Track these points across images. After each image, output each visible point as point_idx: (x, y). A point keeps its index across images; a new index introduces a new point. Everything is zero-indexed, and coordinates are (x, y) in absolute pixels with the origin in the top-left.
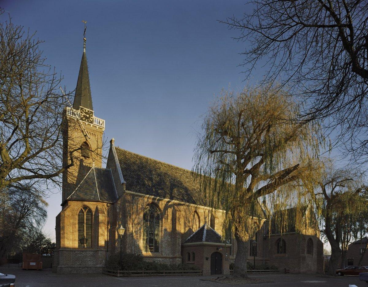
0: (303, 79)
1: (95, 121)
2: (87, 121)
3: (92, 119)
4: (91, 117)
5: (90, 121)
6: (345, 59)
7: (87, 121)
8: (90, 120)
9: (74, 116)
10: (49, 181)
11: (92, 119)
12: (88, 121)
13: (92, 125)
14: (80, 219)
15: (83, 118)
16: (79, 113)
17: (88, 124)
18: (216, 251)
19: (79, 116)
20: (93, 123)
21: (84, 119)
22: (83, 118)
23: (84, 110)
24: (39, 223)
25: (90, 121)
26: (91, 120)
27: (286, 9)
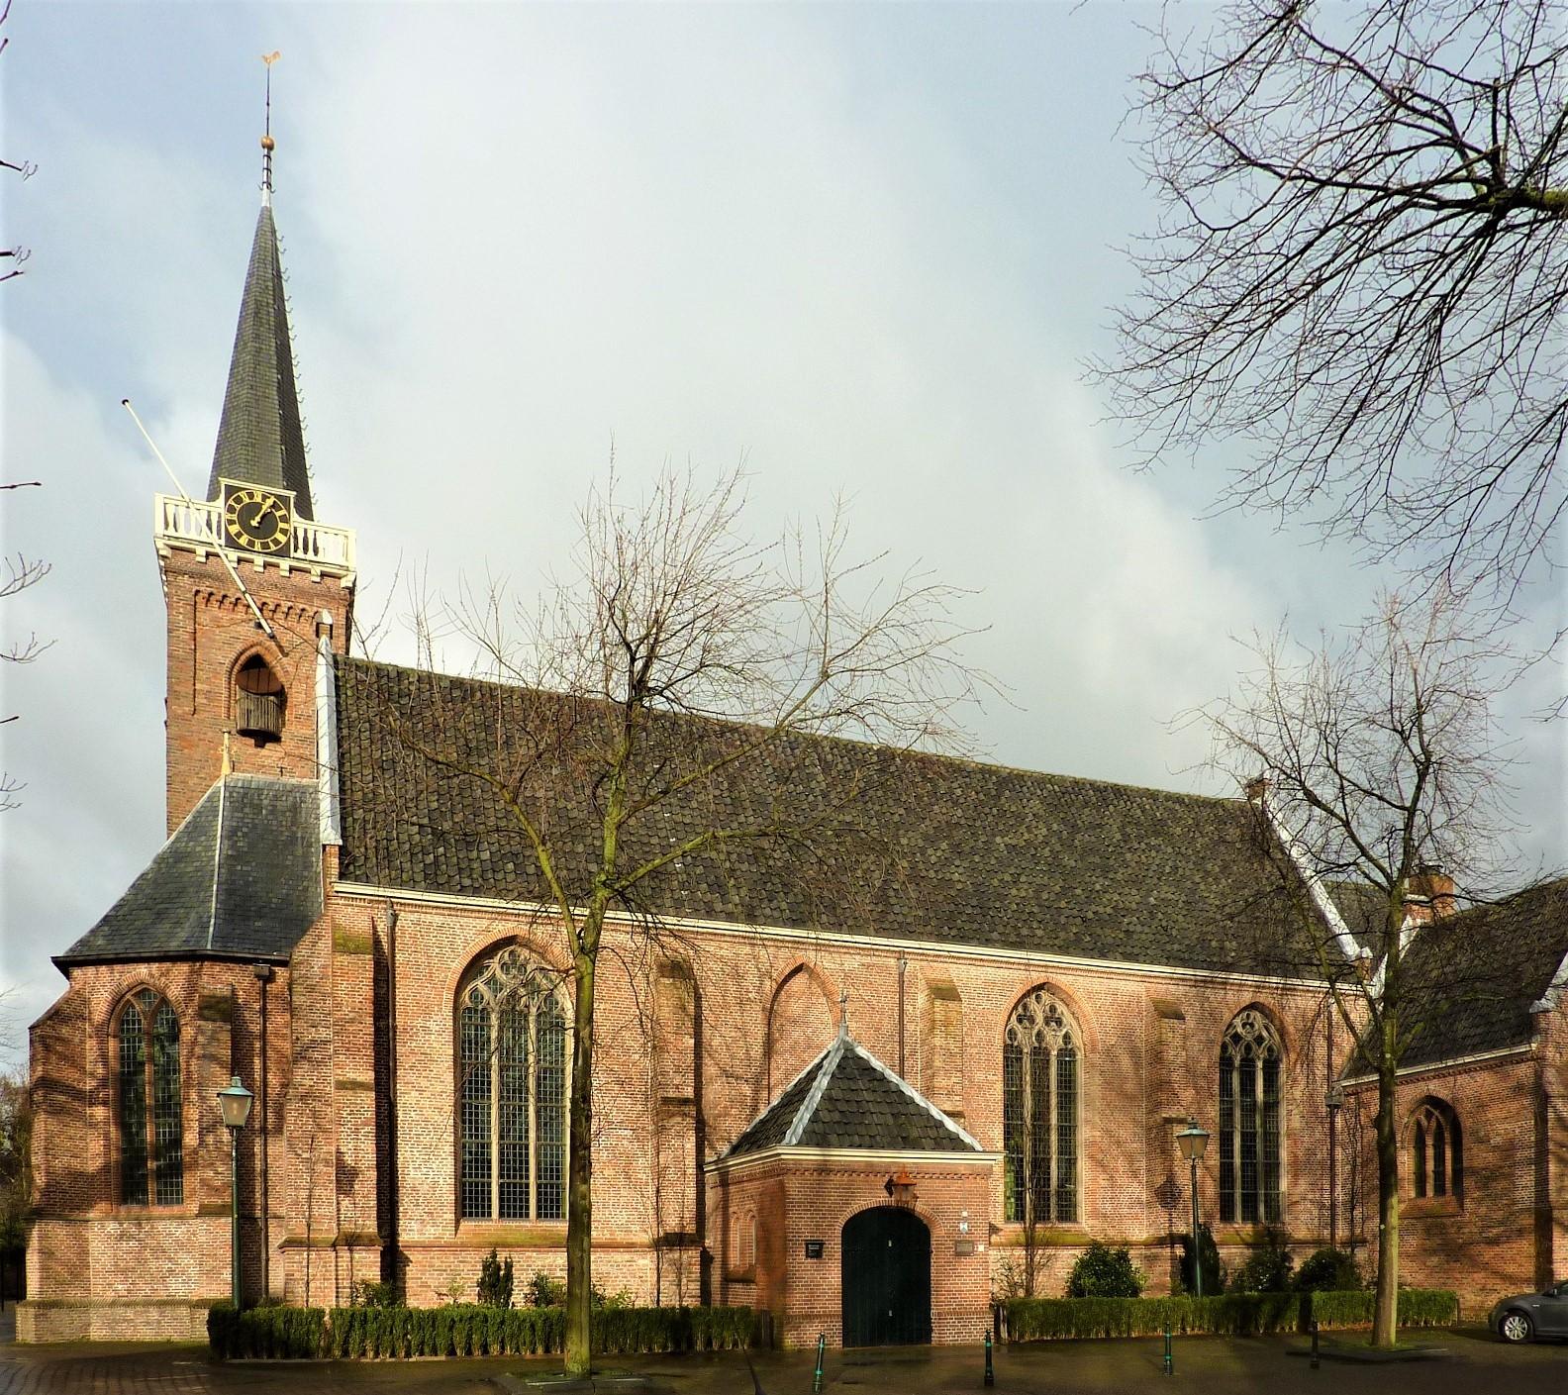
0: (1509, 346)
1: (301, 545)
2: (258, 547)
4: (281, 525)
5: (273, 548)
6: (1183, 163)
7: (258, 547)
8: (276, 542)
9: (310, 555)
10: (778, 1046)
11: (284, 532)
12: (265, 546)
14: (521, 1193)
15: (239, 535)
16: (220, 515)
17: (240, 560)
18: (880, 1198)
19: (219, 533)
20: (292, 554)
21: (243, 541)
22: (239, 535)
23: (242, 494)
24: (472, 1317)
25: (273, 548)
26: (282, 539)
27: (1472, 155)
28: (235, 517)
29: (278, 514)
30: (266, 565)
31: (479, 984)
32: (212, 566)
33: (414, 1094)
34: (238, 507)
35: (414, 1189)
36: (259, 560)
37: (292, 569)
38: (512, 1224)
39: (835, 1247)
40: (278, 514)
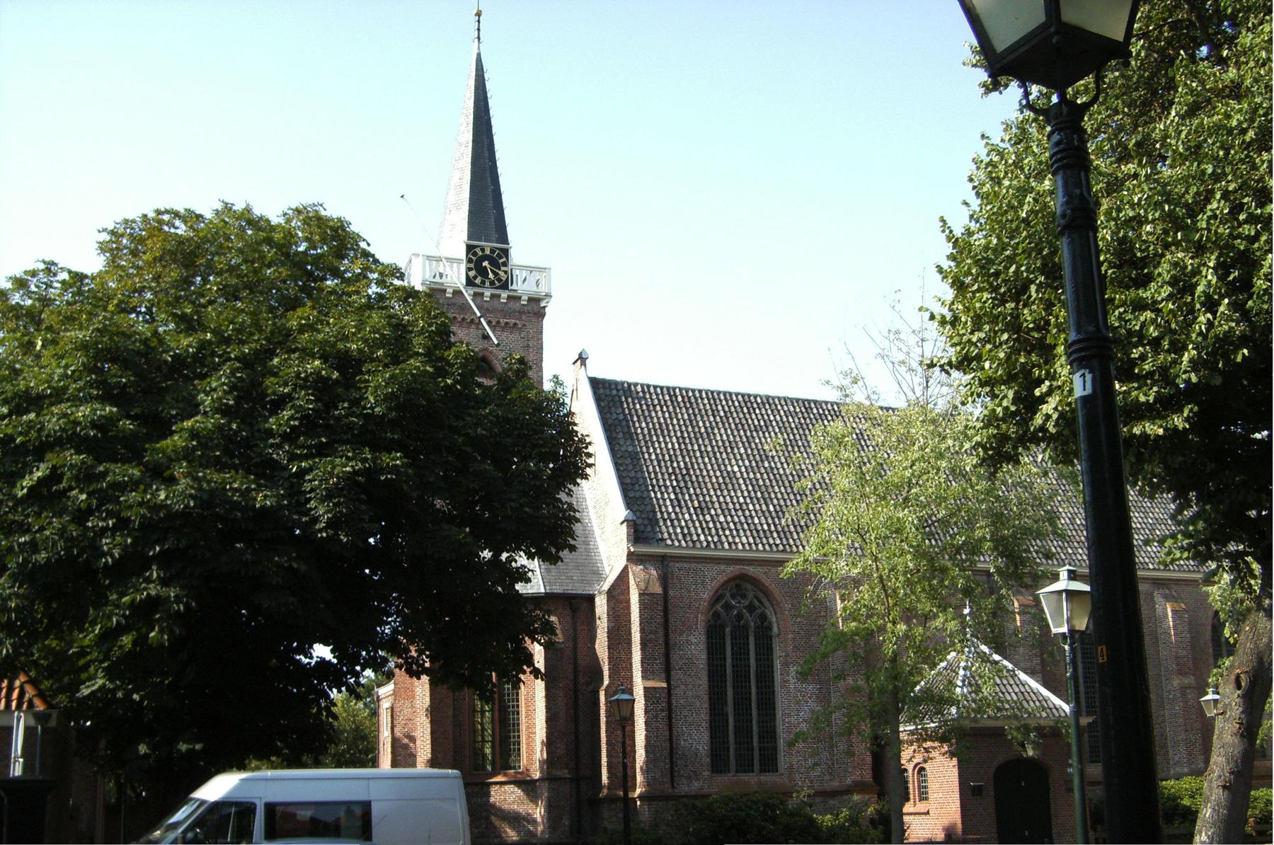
3: (506, 272)
13: (504, 294)
15: (475, 277)
20: (510, 287)
22: (475, 277)
28: (472, 266)
29: (501, 261)
30: (493, 296)
31: (718, 607)
32: (459, 301)
33: (682, 687)
34: (474, 258)
35: (683, 754)
36: (487, 293)
37: (509, 298)
38: (744, 777)
39: (990, 793)
40: (501, 261)
